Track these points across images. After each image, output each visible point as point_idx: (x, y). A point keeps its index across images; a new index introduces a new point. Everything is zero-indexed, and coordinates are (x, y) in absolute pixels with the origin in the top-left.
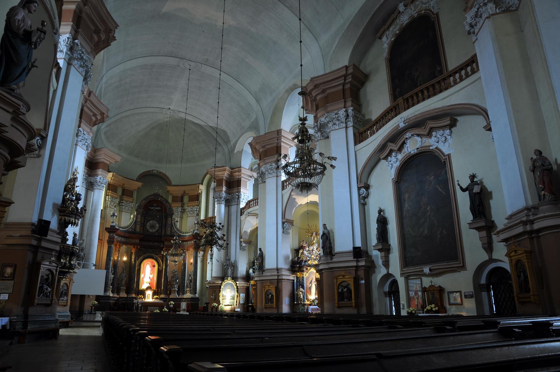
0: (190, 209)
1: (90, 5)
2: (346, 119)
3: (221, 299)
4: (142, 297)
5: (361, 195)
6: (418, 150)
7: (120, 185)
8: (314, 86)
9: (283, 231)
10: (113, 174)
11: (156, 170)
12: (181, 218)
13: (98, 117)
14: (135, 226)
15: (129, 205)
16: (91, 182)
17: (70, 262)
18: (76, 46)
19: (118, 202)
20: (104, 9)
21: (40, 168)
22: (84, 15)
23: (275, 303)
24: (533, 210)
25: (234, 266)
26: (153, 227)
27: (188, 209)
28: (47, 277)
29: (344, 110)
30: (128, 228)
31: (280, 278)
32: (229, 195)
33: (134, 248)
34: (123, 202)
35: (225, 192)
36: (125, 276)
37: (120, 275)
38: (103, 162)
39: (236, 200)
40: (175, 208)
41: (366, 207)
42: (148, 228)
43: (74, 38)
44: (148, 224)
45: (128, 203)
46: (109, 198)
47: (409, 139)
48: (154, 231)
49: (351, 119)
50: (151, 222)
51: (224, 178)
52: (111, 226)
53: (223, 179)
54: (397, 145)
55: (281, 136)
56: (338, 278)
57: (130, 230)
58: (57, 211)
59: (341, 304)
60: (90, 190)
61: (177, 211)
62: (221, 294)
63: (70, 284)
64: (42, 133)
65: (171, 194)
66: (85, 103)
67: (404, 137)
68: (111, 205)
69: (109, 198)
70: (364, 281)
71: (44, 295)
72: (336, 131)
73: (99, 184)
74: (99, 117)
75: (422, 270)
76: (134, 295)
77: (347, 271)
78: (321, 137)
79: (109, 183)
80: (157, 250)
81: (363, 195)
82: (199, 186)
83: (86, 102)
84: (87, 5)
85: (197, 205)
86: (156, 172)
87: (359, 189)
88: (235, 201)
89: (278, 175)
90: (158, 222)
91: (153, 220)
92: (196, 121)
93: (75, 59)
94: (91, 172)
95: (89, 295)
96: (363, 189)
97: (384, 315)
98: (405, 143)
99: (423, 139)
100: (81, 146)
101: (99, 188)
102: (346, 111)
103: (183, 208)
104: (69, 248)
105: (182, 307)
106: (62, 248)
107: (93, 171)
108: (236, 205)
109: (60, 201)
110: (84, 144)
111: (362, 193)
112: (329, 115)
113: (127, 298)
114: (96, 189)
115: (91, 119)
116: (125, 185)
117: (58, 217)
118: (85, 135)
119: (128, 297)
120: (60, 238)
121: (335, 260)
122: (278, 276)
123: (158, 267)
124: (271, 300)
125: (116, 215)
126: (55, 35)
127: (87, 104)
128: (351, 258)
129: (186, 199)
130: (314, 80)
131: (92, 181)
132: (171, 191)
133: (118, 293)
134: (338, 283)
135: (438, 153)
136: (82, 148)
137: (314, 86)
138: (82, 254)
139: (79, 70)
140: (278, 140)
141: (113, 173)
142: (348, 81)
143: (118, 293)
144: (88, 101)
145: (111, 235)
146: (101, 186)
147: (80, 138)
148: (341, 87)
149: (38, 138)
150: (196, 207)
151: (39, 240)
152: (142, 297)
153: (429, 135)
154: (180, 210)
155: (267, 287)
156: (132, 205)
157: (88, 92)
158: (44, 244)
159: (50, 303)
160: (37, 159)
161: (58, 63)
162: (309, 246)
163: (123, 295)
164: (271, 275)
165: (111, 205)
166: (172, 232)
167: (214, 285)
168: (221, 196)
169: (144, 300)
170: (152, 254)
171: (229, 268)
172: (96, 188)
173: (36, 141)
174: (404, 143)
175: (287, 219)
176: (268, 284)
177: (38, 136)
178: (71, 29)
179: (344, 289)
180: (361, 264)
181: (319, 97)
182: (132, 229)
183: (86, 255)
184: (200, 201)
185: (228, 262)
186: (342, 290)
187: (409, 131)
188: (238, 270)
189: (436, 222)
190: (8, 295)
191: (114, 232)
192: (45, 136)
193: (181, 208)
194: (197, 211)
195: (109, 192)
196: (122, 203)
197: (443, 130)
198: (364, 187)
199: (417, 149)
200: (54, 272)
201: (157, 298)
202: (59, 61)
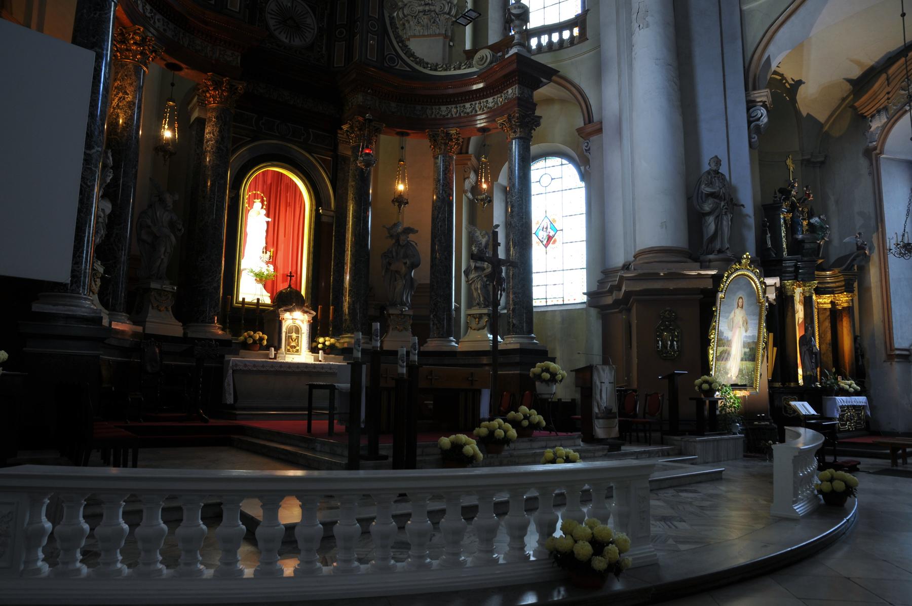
9: (845, 95)
33: (217, 85)
36: (172, 225)
76: (217, 330)
105: (598, 397)
113: (185, 339)
119: (189, 335)
123: (317, 211)
143: (135, 312)
152: (261, 339)
167: (671, 285)
170: (289, 145)
189: (257, 324)
194: (449, 14)
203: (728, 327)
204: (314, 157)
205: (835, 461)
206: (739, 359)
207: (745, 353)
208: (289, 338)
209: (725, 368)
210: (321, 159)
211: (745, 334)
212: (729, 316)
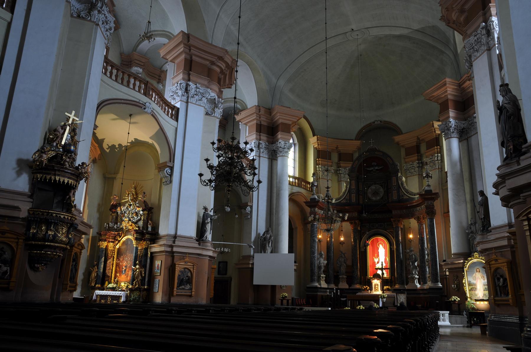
0: (430, 160)
3: (467, 289)
4: (368, 289)
10: (318, 138)
11: (379, 120)
14: (350, 196)
26: (376, 193)
32: (464, 122)
35: (455, 118)
38: (282, 123)
40: (410, 164)
42: (370, 195)
44: (370, 190)
48: (378, 198)
50: (373, 187)
51: (450, 97)
53: (447, 100)
57: (344, 201)
62: (465, 281)
65: (403, 146)
66: (190, 52)
68: (323, 175)
76: (358, 286)
79: (318, 149)
80: (385, 223)
82: (433, 124)
85: (437, 152)
86: (379, 122)
90: (382, 186)
91: (376, 184)
92: (397, 32)
95: (281, 286)
97: (439, 323)
101: (281, 155)
103: (420, 161)
104: (52, 215)
106: (32, 214)
113: (349, 289)
116: (339, 148)
117: (29, 177)
118: (199, 88)
119: (350, 288)
120: (31, 202)
129: (423, 148)
131: (274, 148)
132: (400, 143)
141: (317, 136)
145: (313, 210)
154: (416, 164)
155: (494, 266)
162: (214, 110)
163: (344, 285)
165: (323, 175)
168: (448, 126)
169: (370, 292)
184: (441, 145)
195: (319, 161)
196: (340, 170)
201: (388, 290)
203: (473, 279)
204: (388, 232)
205: (67, 246)
206: (482, 290)
207: (485, 288)
208: (375, 287)
209: (475, 294)
210: (389, 231)
211: (483, 281)
212: (473, 275)
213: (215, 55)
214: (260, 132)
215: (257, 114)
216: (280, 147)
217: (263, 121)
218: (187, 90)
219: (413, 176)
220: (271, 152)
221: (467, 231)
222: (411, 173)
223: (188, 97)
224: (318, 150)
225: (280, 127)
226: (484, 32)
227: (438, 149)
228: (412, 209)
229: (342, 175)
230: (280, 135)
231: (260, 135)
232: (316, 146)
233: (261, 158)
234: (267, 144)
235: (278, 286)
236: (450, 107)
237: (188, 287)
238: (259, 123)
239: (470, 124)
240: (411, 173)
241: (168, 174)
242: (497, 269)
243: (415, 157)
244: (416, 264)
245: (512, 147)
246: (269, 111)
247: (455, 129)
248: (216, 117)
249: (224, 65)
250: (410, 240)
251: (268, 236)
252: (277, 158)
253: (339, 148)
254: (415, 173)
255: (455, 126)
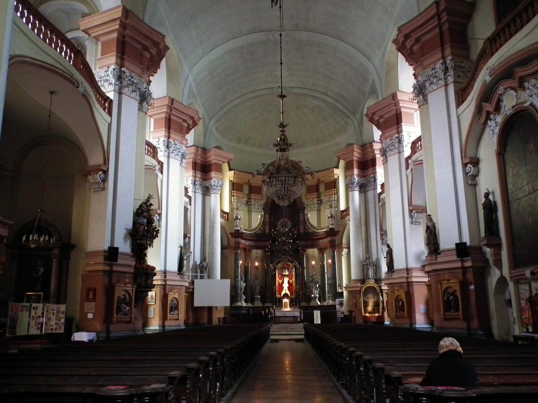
0: (328, 199)
1: (129, 27)
2: (445, 74)
5: (468, 173)
6: (514, 108)
7: (246, 183)
8: (404, 37)
10: (234, 172)
12: (318, 211)
13: (189, 122)
14: (264, 227)
15: (259, 204)
16: (207, 187)
17: (146, 281)
18: (123, 73)
19: (245, 202)
20: (144, 26)
21: (106, 200)
22: (127, 39)
23: (406, 312)
24: (138, 281)
25: (376, 266)
26: (284, 225)
27: (324, 199)
28: (124, 297)
29: (441, 62)
30: (257, 230)
31: (410, 280)
32: (363, 179)
34: (251, 200)
35: (359, 176)
37: (253, 282)
38: (216, 164)
39: (373, 184)
41: (477, 188)
43: (122, 66)
45: (257, 201)
46: (234, 198)
47: (504, 95)
49: (451, 72)
52: (235, 230)
54: (492, 104)
55: (397, 100)
56: (442, 283)
57: (259, 232)
58: (129, 237)
59: (448, 316)
60: (207, 195)
61: (313, 203)
63: (179, 298)
64: (102, 168)
66: (170, 112)
67: (497, 93)
69: (234, 198)
70: (473, 286)
71: (123, 313)
72: (434, 92)
73: (214, 187)
74: (190, 122)
75: (522, 273)
77: (454, 274)
78: (423, 101)
81: (470, 173)
82: (333, 170)
83: (171, 111)
84: (127, 29)
85: (334, 193)
87: (465, 165)
88: (371, 185)
89: (401, 151)
90: (290, 219)
93: (125, 86)
94: (206, 176)
96: (470, 166)
98: (502, 101)
99: (518, 93)
100: (174, 157)
101: (214, 192)
102: (444, 63)
103: (319, 199)
107: (207, 174)
108: (373, 190)
109: (130, 226)
110: (178, 155)
111: (469, 171)
112: (424, 73)
114: (212, 193)
115: (182, 126)
116: (250, 182)
118: (177, 145)
119: (264, 306)
121: (440, 259)
122: (407, 278)
124: (402, 308)
125: (239, 218)
126: (78, 89)
127: (173, 112)
128: (455, 258)
129: (322, 188)
130: (402, 29)
131: (207, 185)
133: (252, 302)
134: (443, 289)
135: (531, 109)
136: (176, 159)
137: (404, 37)
138: (205, 264)
139: (132, 96)
140: (395, 106)
142: (443, 20)
143: (252, 302)
144: (173, 109)
146: (217, 190)
147: (172, 149)
148: (437, 30)
149: (100, 173)
150: (334, 196)
151: (111, 266)
153: (521, 86)
154: (315, 201)
155: (396, 293)
156: (258, 203)
157: (171, 100)
158: (116, 268)
159: (130, 320)
160: (103, 192)
161: (108, 97)
163: (258, 304)
164: (399, 278)
166: (306, 230)
168: (352, 181)
171: (369, 269)
172: (212, 192)
173: (99, 177)
174: (499, 101)
175: (414, 206)
176: (397, 288)
177: (100, 171)
178: (116, 59)
179: (451, 296)
180: (468, 264)
181: (415, 48)
182: (261, 230)
183: (209, 265)
184: (337, 187)
185: (368, 261)
186: (448, 298)
187: (500, 84)
188: (381, 270)
190: (92, 314)
191: (238, 237)
192: (106, 169)
193: (317, 199)
194: (335, 200)
195: (234, 193)
196: (250, 202)
197: (534, 78)
198: (470, 163)
199: (513, 107)
200: (131, 292)
202: (108, 95)
208: (285, 305)
213: (188, 115)
214: (195, 170)
215: (194, 153)
216: (214, 185)
217: (198, 159)
218: (168, 147)
219: (313, 211)
220: (203, 188)
221: (363, 264)
222: (311, 208)
223: (169, 153)
224: (232, 183)
225: (213, 167)
226: (397, 140)
227: (336, 191)
228: (315, 241)
229: (252, 206)
230: (213, 174)
231: (195, 173)
232: (232, 179)
233: (197, 193)
234: (201, 180)
235: (214, 307)
236: (354, 167)
237: (176, 312)
238: (194, 161)
239: (368, 181)
240: (311, 208)
241: (157, 220)
242: (398, 295)
243: (315, 195)
244: (317, 286)
245: (433, 248)
246: (205, 150)
247: (357, 184)
248: (183, 167)
249: (192, 121)
250: (313, 266)
251: (205, 264)
252: (210, 194)
253: (250, 182)
254: (314, 208)
255: (357, 181)
